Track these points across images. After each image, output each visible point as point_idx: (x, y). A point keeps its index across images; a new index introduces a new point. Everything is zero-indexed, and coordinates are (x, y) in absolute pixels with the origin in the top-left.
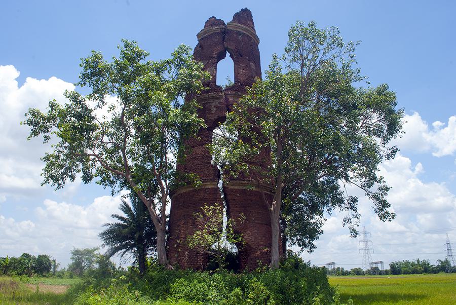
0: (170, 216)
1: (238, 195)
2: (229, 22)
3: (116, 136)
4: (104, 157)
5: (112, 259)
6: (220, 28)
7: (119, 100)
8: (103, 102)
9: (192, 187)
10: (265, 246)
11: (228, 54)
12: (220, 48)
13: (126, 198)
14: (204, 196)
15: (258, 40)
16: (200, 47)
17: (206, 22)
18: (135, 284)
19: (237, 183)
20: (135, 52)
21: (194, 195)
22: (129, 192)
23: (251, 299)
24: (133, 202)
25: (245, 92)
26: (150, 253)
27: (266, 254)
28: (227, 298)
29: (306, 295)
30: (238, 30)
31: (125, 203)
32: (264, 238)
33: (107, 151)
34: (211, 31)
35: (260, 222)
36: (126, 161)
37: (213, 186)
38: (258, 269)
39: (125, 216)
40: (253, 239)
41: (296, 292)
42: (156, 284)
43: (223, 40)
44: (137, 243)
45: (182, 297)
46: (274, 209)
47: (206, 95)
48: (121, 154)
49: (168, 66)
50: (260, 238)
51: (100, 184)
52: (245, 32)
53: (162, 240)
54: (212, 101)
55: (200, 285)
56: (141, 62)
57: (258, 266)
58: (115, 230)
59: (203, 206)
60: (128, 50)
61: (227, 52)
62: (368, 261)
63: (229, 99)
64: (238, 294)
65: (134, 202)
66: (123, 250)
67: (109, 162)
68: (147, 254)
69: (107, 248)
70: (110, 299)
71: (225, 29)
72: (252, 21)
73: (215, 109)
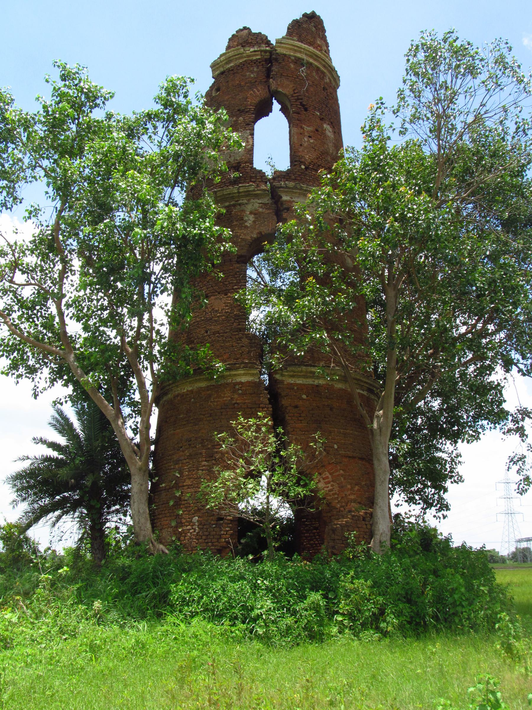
0: (156, 442)
1: (304, 397)
2: (280, 37)
3: (41, 271)
4: (15, 315)
5: (31, 533)
6: (261, 51)
7: (50, 190)
8: (15, 198)
9: (207, 379)
10: (360, 503)
11: (276, 106)
12: (259, 93)
13: (62, 404)
14: (232, 398)
15: (267, 115)
16: (218, 90)
17: (230, 40)
18: (88, 584)
19: (301, 371)
20: (82, 92)
21: (210, 396)
22: (70, 390)
23: (343, 614)
24: (78, 413)
25: (317, 181)
26: (115, 519)
27: (364, 519)
28: (294, 613)
29: (463, 606)
30: (298, 55)
31: (61, 413)
32: (357, 488)
33: (22, 303)
34: (242, 58)
35: (349, 454)
36: (63, 323)
37: (250, 379)
38: (348, 553)
39: (62, 441)
40: (336, 489)
41: (439, 599)
42: (135, 584)
43: (268, 76)
44: (86, 499)
45: (197, 613)
46: (380, 428)
47: (234, 189)
48: (53, 310)
49: (149, 126)
50: (349, 486)
51: (7, 374)
52: (311, 60)
53: (141, 491)
54: (245, 201)
55: (237, 586)
56: (98, 115)
57: (347, 545)
58: (39, 469)
59: (236, 418)
60: (69, 87)
61: (275, 102)
62: (512, 536)
63: (281, 197)
64: (318, 605)
65: (80, 414)
66: (57, 513)
67: (25, 326)
68: (107, 520)
69: (24, 506)
70: (37, 618)
71: (270, 52)
72: (324, 38)
73: (252, 218)
